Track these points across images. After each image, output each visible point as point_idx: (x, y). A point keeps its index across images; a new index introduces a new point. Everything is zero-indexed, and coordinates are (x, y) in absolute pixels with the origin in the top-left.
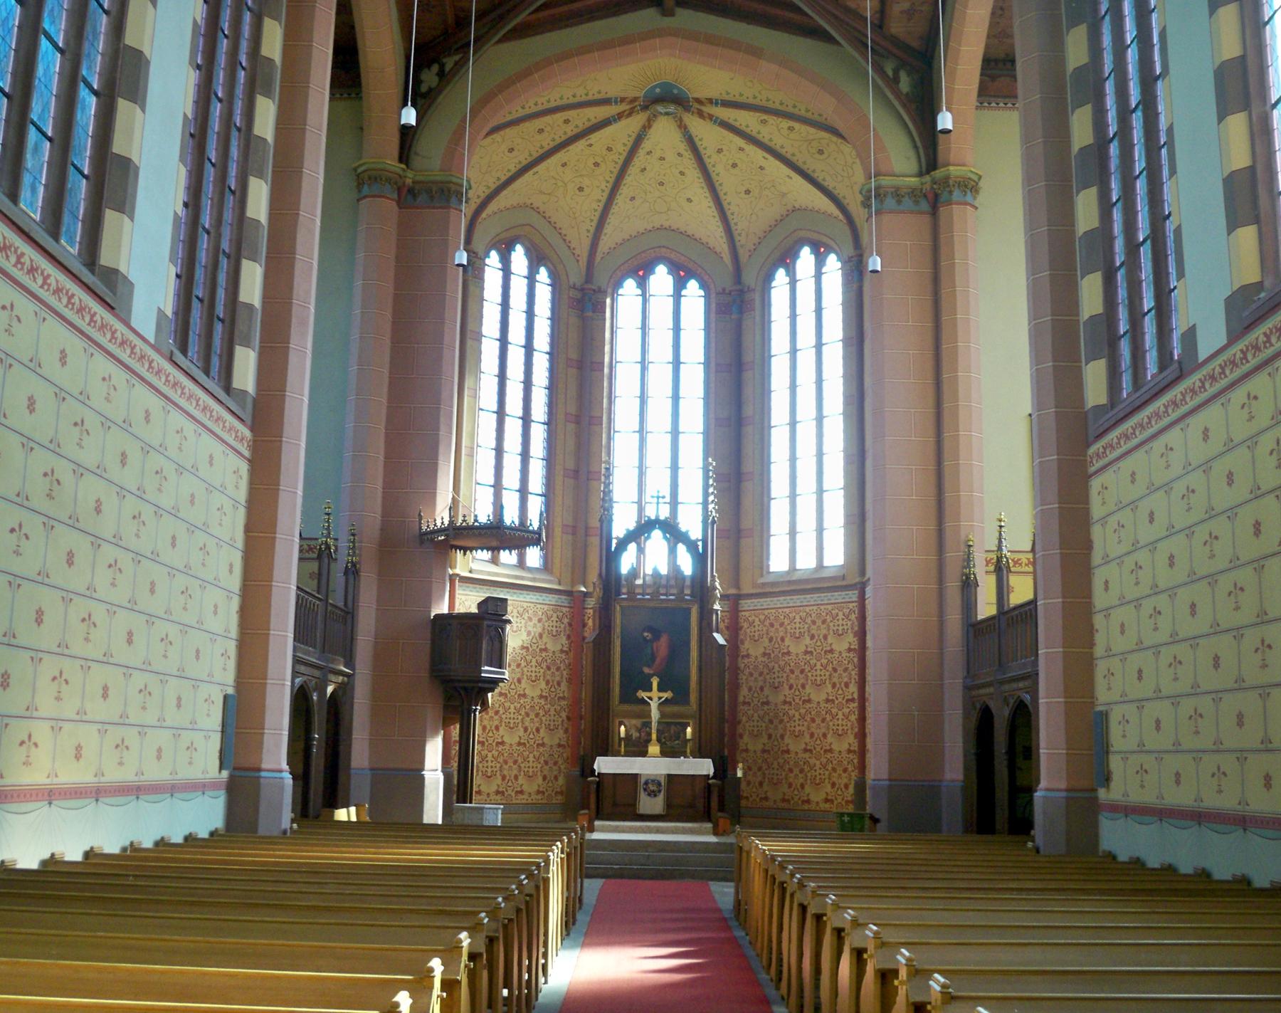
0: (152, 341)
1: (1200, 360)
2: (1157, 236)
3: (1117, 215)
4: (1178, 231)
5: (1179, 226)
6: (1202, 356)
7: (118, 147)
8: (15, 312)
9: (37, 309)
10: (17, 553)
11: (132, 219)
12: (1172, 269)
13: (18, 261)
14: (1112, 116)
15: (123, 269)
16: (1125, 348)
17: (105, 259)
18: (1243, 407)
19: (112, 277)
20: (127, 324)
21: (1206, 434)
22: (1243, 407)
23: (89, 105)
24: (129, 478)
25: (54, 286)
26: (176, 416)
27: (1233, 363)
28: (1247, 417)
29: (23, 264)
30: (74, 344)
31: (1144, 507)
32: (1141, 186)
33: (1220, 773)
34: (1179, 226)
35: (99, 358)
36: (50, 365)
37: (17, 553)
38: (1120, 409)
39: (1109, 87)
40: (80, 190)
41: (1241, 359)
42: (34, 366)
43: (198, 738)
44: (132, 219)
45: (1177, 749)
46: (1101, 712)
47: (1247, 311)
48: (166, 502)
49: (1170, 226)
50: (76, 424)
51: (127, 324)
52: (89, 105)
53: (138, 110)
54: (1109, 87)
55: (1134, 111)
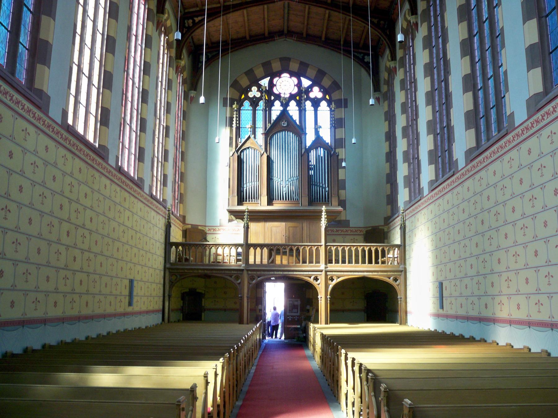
0: (60, 123)
1: (516, 126)
2: (496, 76)
3: (478, 66)
4: (506, 73)
5: (506, 71)
6: (459, 169)
7: (42, 36)
8: (27, 131)
9: (14, 115)
10: (6, 219)
11: (49, 68)
12: (502, 88)
13: (53, 129)
14: (475, 24)
15: (45, 89)
16: (482, 122)
17: (37, 86)
18: (548, 137)
19: (40, 93)
20: (47, 115)
21: (529, 152)
22: (548, 137)
23: (27, 18)
24: (111, 215)
25: (59, 135)
26: (114, 186)
27: (502, 147)
28: (550, 142)
29: (10, 96)
30: (52, 144)
31: (485, 194)
32: (488, 54)
33: (473, 303)
34: (506, 71)
35: (20, 120)
36: (76, 174)
37: (6, 219)
38: (481, 150)
39: (474, 12)
40: (23, 53)
41: (544, 116)
42: (12, 138)
43: (122, 298)
44: (49, 68)
45: (472, 295)
46: (201, 316)
47: (536, 104)
48: (73, 197)
49: (502, 70)
50: (32, 164)
51: (47, 115)
52: (27, 18)
53: (52, 20)
54: (474, 12)
55: (475, 35)
